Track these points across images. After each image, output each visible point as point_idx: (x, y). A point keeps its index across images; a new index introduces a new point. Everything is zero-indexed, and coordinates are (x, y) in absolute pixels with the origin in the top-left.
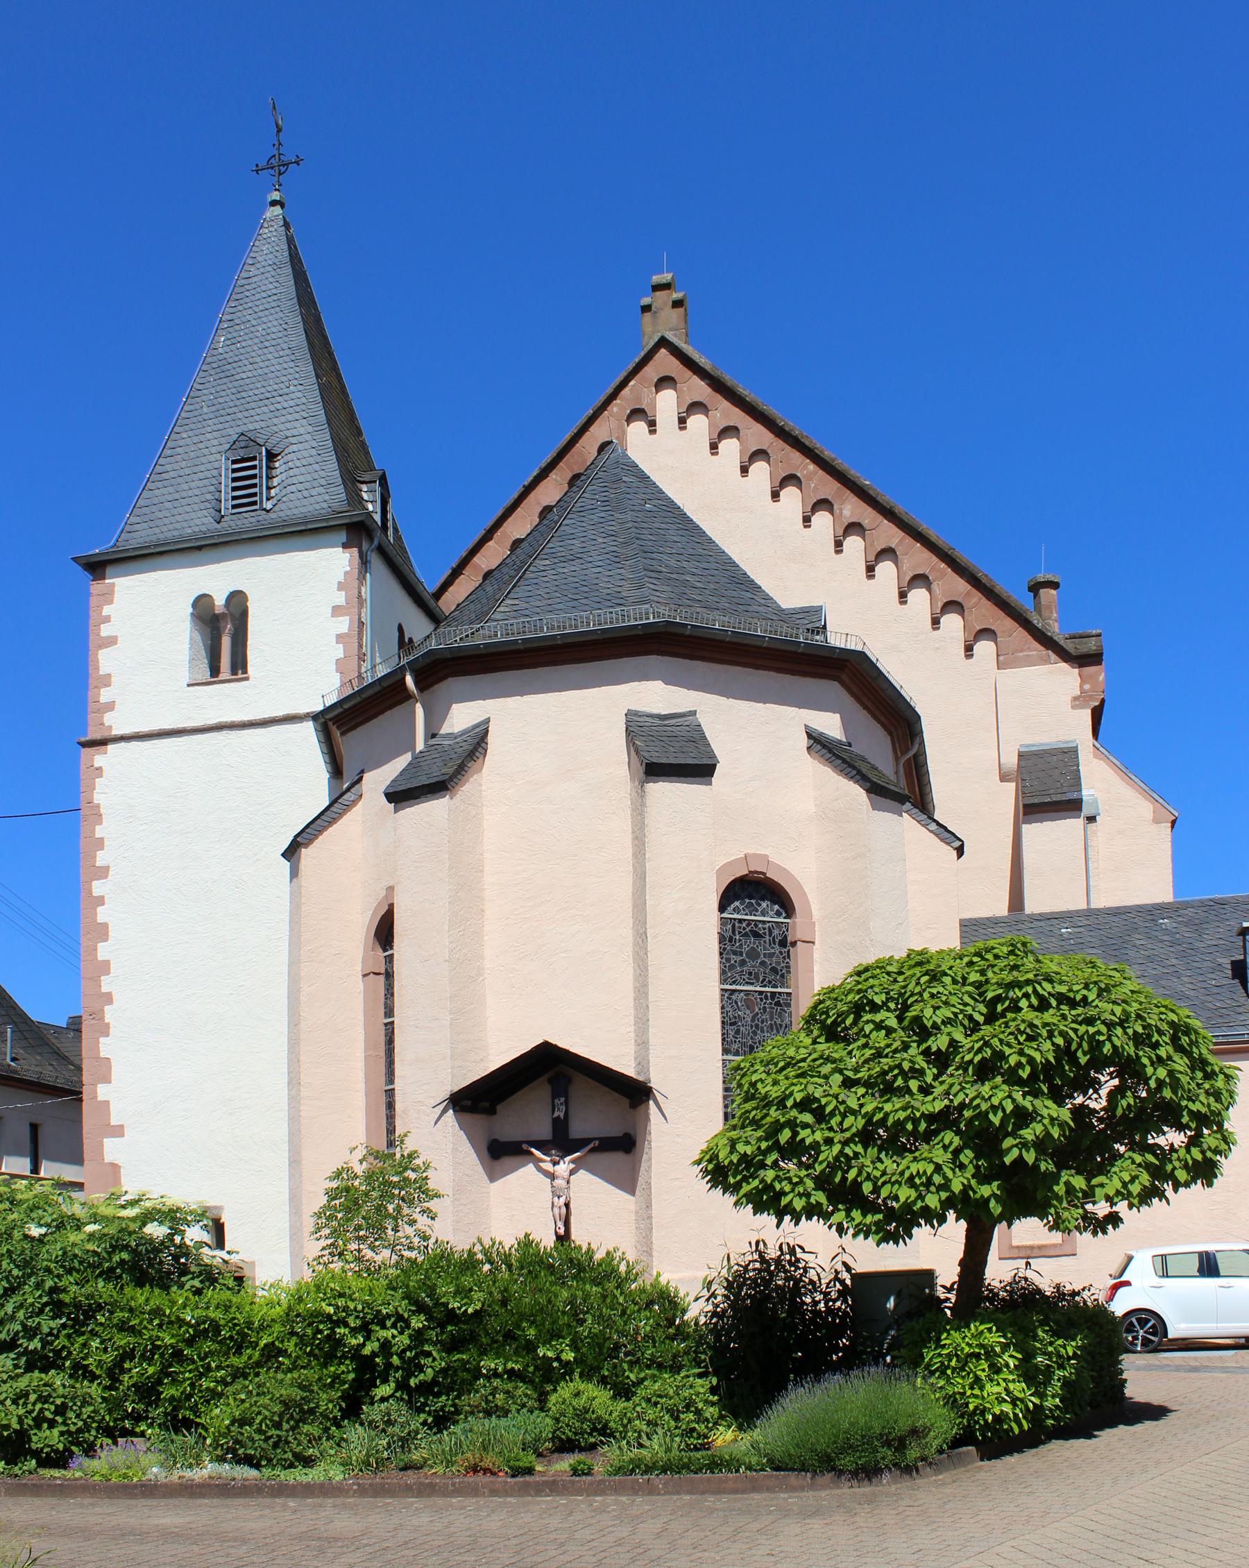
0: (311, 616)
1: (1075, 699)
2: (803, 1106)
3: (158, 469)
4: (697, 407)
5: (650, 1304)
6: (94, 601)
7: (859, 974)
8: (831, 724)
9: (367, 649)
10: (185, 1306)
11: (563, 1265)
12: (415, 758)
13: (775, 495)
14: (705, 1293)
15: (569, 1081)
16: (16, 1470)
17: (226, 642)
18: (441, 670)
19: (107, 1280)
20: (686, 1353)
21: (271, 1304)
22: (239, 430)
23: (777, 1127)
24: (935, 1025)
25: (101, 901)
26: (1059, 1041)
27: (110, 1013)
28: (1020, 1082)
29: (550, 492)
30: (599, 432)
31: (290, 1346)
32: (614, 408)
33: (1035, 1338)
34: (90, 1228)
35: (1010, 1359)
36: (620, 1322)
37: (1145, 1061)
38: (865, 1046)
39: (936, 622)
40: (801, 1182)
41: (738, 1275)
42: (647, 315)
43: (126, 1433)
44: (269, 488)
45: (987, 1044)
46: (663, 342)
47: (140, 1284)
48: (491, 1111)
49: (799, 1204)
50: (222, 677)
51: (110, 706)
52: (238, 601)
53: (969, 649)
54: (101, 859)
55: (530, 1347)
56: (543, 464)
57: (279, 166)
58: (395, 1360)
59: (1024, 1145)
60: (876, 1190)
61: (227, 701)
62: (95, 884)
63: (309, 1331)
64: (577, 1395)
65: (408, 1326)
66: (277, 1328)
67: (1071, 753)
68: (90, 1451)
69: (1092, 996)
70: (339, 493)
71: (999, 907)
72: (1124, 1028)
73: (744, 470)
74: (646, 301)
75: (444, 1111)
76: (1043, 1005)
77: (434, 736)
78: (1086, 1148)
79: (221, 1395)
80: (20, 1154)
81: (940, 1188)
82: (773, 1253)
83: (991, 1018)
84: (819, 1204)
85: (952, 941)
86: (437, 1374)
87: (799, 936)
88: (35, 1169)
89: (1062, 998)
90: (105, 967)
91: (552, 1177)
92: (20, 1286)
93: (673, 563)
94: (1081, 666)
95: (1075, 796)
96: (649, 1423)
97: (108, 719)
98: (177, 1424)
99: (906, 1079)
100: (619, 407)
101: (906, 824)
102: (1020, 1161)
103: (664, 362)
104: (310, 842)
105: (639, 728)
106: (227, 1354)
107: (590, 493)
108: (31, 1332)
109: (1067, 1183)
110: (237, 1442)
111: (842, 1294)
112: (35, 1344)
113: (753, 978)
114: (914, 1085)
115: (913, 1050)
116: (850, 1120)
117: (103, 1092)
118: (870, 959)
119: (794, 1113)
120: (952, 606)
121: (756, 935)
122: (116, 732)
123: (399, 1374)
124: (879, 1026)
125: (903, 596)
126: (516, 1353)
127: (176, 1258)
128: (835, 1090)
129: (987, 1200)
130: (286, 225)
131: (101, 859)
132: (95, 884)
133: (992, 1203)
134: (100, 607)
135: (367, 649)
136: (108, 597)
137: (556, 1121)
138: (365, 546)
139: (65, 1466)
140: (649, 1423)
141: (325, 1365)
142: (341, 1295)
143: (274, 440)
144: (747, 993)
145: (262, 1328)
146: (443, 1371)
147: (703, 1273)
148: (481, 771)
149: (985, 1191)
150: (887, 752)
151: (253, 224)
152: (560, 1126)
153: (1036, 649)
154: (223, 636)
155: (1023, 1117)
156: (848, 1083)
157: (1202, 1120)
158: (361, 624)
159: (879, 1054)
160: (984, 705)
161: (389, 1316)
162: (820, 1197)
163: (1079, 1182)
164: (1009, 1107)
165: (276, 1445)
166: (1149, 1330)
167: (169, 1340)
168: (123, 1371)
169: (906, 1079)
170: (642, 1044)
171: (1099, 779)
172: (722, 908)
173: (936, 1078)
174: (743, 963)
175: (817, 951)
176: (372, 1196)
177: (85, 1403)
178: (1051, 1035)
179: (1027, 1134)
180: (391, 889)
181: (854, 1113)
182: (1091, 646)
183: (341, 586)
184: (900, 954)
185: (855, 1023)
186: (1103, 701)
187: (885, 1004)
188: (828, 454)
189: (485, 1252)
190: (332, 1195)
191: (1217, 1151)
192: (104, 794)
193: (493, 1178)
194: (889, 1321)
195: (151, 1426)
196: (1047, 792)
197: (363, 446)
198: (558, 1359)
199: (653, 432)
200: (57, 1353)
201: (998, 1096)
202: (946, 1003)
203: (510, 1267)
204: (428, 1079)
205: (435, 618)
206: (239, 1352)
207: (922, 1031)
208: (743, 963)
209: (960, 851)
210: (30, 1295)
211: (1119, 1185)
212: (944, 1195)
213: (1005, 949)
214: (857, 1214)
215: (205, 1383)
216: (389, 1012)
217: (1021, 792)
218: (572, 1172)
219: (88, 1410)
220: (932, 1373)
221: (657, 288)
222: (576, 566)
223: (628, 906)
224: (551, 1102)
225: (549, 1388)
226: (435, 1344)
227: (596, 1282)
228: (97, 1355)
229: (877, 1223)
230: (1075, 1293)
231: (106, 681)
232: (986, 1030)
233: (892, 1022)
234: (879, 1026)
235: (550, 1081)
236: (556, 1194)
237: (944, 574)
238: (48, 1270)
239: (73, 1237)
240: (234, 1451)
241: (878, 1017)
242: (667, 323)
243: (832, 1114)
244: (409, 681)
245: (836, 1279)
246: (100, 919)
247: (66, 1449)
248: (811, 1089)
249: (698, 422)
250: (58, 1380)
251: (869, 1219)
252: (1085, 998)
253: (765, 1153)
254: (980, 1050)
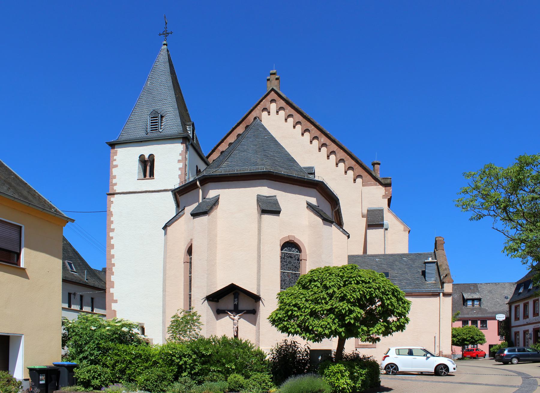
0: (172, 162)
1: (383, 196)
2: (295, 305)
3: (130, 118)
4: (281, 108)
5: (256, 355)
6: (111, 155)
7: (311, 272)
8: (313, 201)
9: (187, 172)
10: (132, 349)
11: (236, 343)
12: (199, 204)
13: (303, 135)
14: (271, 353)
15: (239, 294)
16: (87, 390)
17: (148, 168)
18: (207, 180)
19: (112, 342)
20: (265, 368)
21: (156, 350)
22: (153, 109)
23: (288, 311)
24: (330, 287)
25: (112, 238)
26: (361, 292)
27: (114, 269)
28: (351, 302)
29: (240, 130)
30: (254, 114)
31: (160, 361)
32: (259, 107)
33: (354, 369)
34: (108, 328)
35: (347, 374)
36: (248, 359)
37: (384, 298)
38: (312, 291)
39: (346, 172)
40: (294, 325)
41: (280, 348)
42: (269, 82)
43: (116, 382)
44: (161, 126)
45: (342, 292)
46: (273, 90)
47: (121, 343)
48: (217, 301)
49: (293, 331)
50: (147, 178)
51: (116, 184)
52: (152, 156)
53: (355, 180)
54: (112, 226)
55: (224, 365)
56: (238, 122)
57: (166, 34)
58: (188, 366)
59: (351, 319)
60: (313, 328)
61: (148, 184)
62: (111, 233)
63: (165, 358)
64: (235, 377)
65: (192, 357)
66: (157, 356)
67: (381, 211)
68: (107, 386)
69: (371, 281)
70: (180, 128)
71: (361, 252)
72: (379, 290)
73: (294, 127)
74: (268, 78)
75: (205, 301)
76: (358, 283)
77: (204, 198)
78: (370, 320)
79: (142, 373)
80: (88, 306)
81: (329, 329)
82: (289, 343)
83: (344, 286)
84: (298, 331)
85: (345, 262)
86: (199, 370)
87: (303, 258)
88: (92, 310)
89: (363, 281)
90: (113, 256)
91: (233, 320)
92: (89, 342)
93: (272, 154)
95: (382, 223)
96: (253, 385)
97: (115, 188)
98: (130, 380)
99: (321, 300)
101: (334, 228)
102: (350, 323)
103: (273, 95)
104: (170, 225)
105: (260, 199)
106: (143, 363)
107: (250, 132)
108: (92, 355)
109: (362, 329)
110: (145, 385)
111: (307, 355)
112: (93, 358)
113: (290, 269)
114: (323, 301)
115: (323, 293)
116: (307, 310)
117: (112, 290)
118: (314, 268)
119: (293, 307)
120: (350, 168)
121: (291, 257)
122: (117, 191)
123: (189, 370)
124: (315, 286)
125: (337, 164)
126: (220, 366)
127: (131, 337)
128: (303, 302)
129: (341, 332)
130: (168, 51)
131: (112, 226)
132: (111, 233)
133: (342, 333)
134: (113, 156)
135: (187, 172)
136: (116, 153)
137: (235, 305)
138: (187, 143)
139: (100, 390)
140: (253, 385)
141: (169, 367)
142: (174, 349)
143: (162, 112)
144: (288, 273)
145: (153, 356)
146: (201, 370)
147: (271, 347)
149: (341, 330)
150: (330, 210)
151: (158, 50)
152: (236, 306)
153: (373, 181)
154: (147, 166)
155: (351, 312)
156: (307, 300)
157: (400, 315)
158: (186, 165)
159: (315, 293)
160: (357, 196)
161: (186, 355)
162: (299, 329)
163: (365, 329)
164: (347, 309)
165: (156, 387)
166: (392, 369)
167: (128, 358)
168: (116, 366)
169: (321, 300)
170: (259, 285)
171: (389, 218)
172: (282, 250)
173: (329, 300)
174: (287, 265)
176: (183, 323)
177: (106, 374)
178: (359, 291)
179: (352, 316)
180: (192, 239)
181: (308, 308)
182: (388, 181)
183: (180, 154)
184: (323, 267)
185: (310, 284)
186: (391, 197)
187: (317, 280)
188: (317, 124)
189: (213, 339)
190: (173, 322)
191: (404, 323)
192: (113, 208)
193: (217, 319)
194: (318, 362)
195: (123, 380)
196: (374, 221)
197: (188, 114)
198: (231, 368)
199: (269, 115)
200: (99, 360)
201: (344, 306)
202: (333, 281)
203: (219, 343)
204: (200, 292)
205: (207, 164)
206: (147, 362)
207: (326, 288)
208: (287, 265)
209: (349, 237)
210: (92, 345)
211: (376, 330)
212: (330, 330)
213: (350, 267)
214: (308, 334)
215: (137, 370)
216: (190, 273)
217: (367, 221)
218: (239, 319)
219: (106, 375)
220: (326, 376)
221: (272, 74)
222: (245, 153)
223: (256, 248)
224: (232, 300)
225: (228, 375)
226: (199, 362)
227: (242, 348)
228: (109, 361)
229: (313, 337)
230: (369, 358)
231: (115, 177)
232: (342, 289)
233: (319, 285)
234: (315, 286)
235: (234, 294)
236: (234, 324)
238: (96, 338)
239: (103, 330)
240: (145, 387)
241: (315, 284)
242: (274, 84)
243: (302, 308)
244: (198, 183)
245: (305, 351)
246: (112, 243)
247: (101, 385)
248: (297, 301)
249: (282, 113)
250: (99, 367)
251: (311, 336)
252: (369, 282)
253: (285, 317)
254: (340, 294)
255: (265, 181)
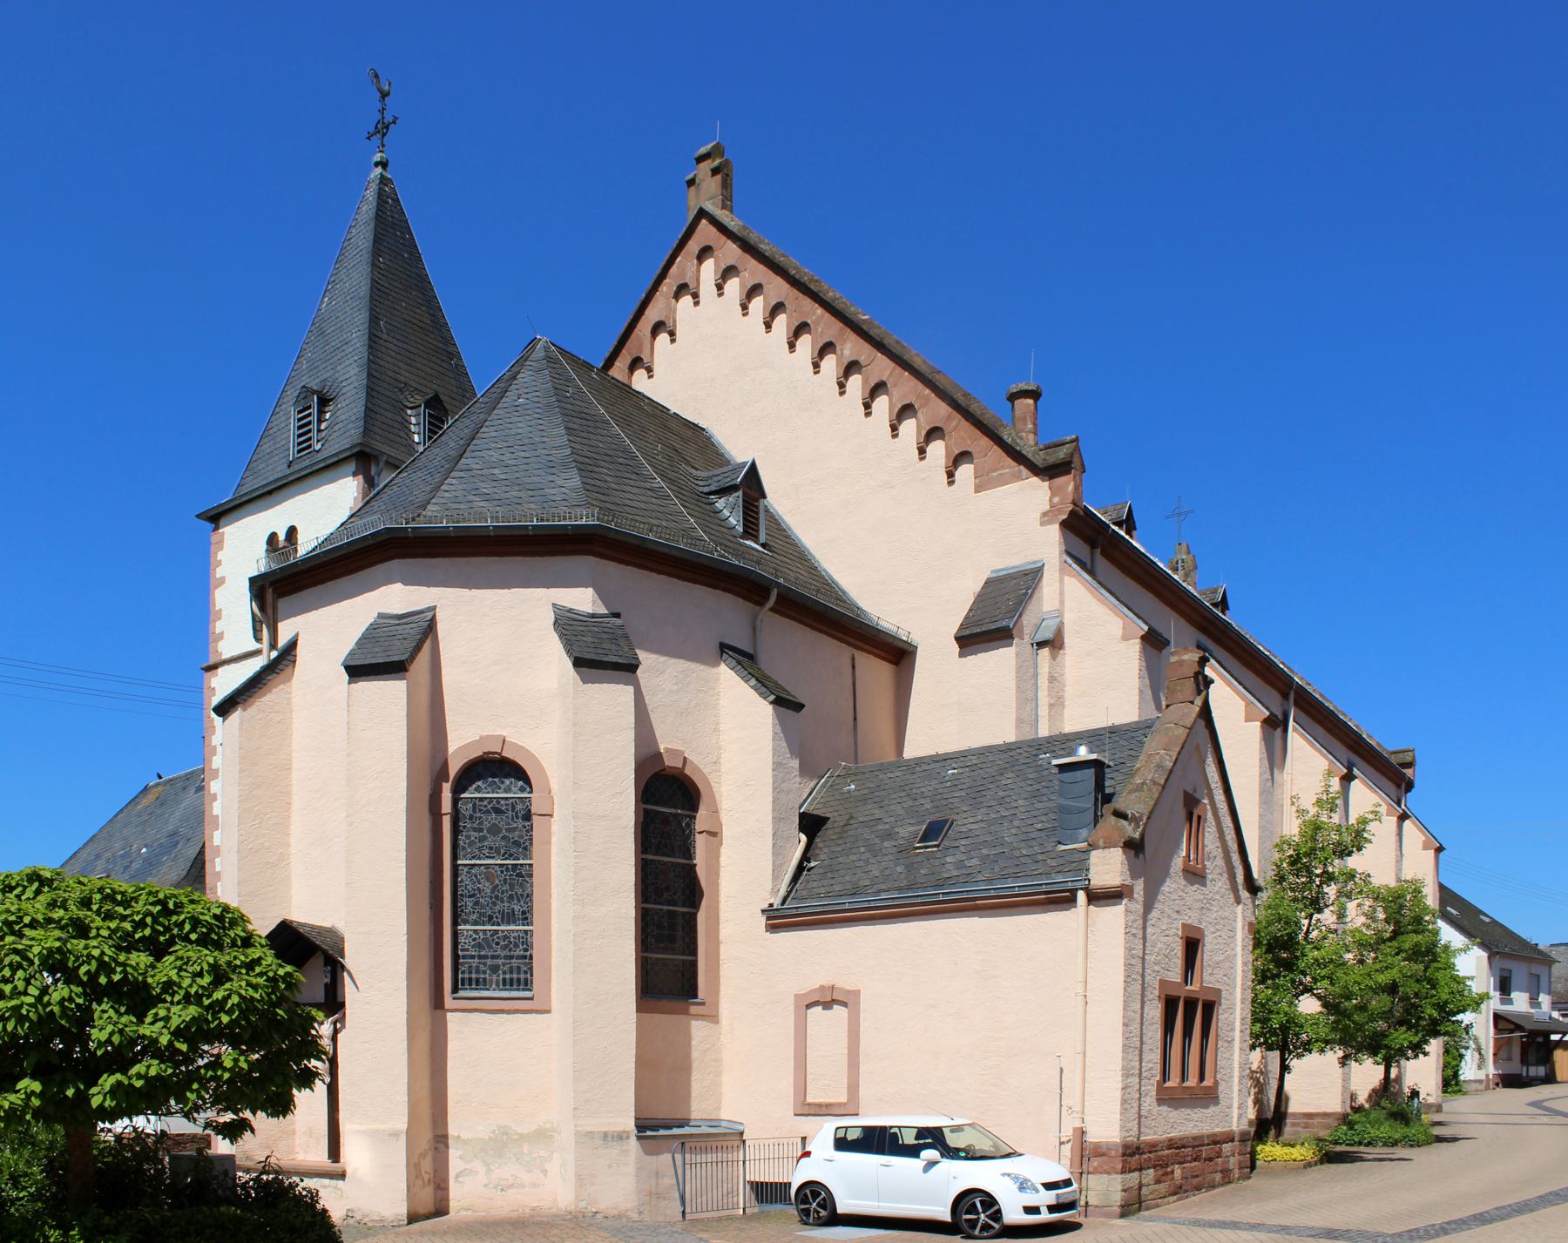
1: (1045, 514)
6: (213, 548)
94: (1051, 478)
100: (668, 286)
103: (705, 231)
122: (225, 656)
148: (290, 678)
175: (556, 824)
237: (928, 400)
255: (395, 565)
